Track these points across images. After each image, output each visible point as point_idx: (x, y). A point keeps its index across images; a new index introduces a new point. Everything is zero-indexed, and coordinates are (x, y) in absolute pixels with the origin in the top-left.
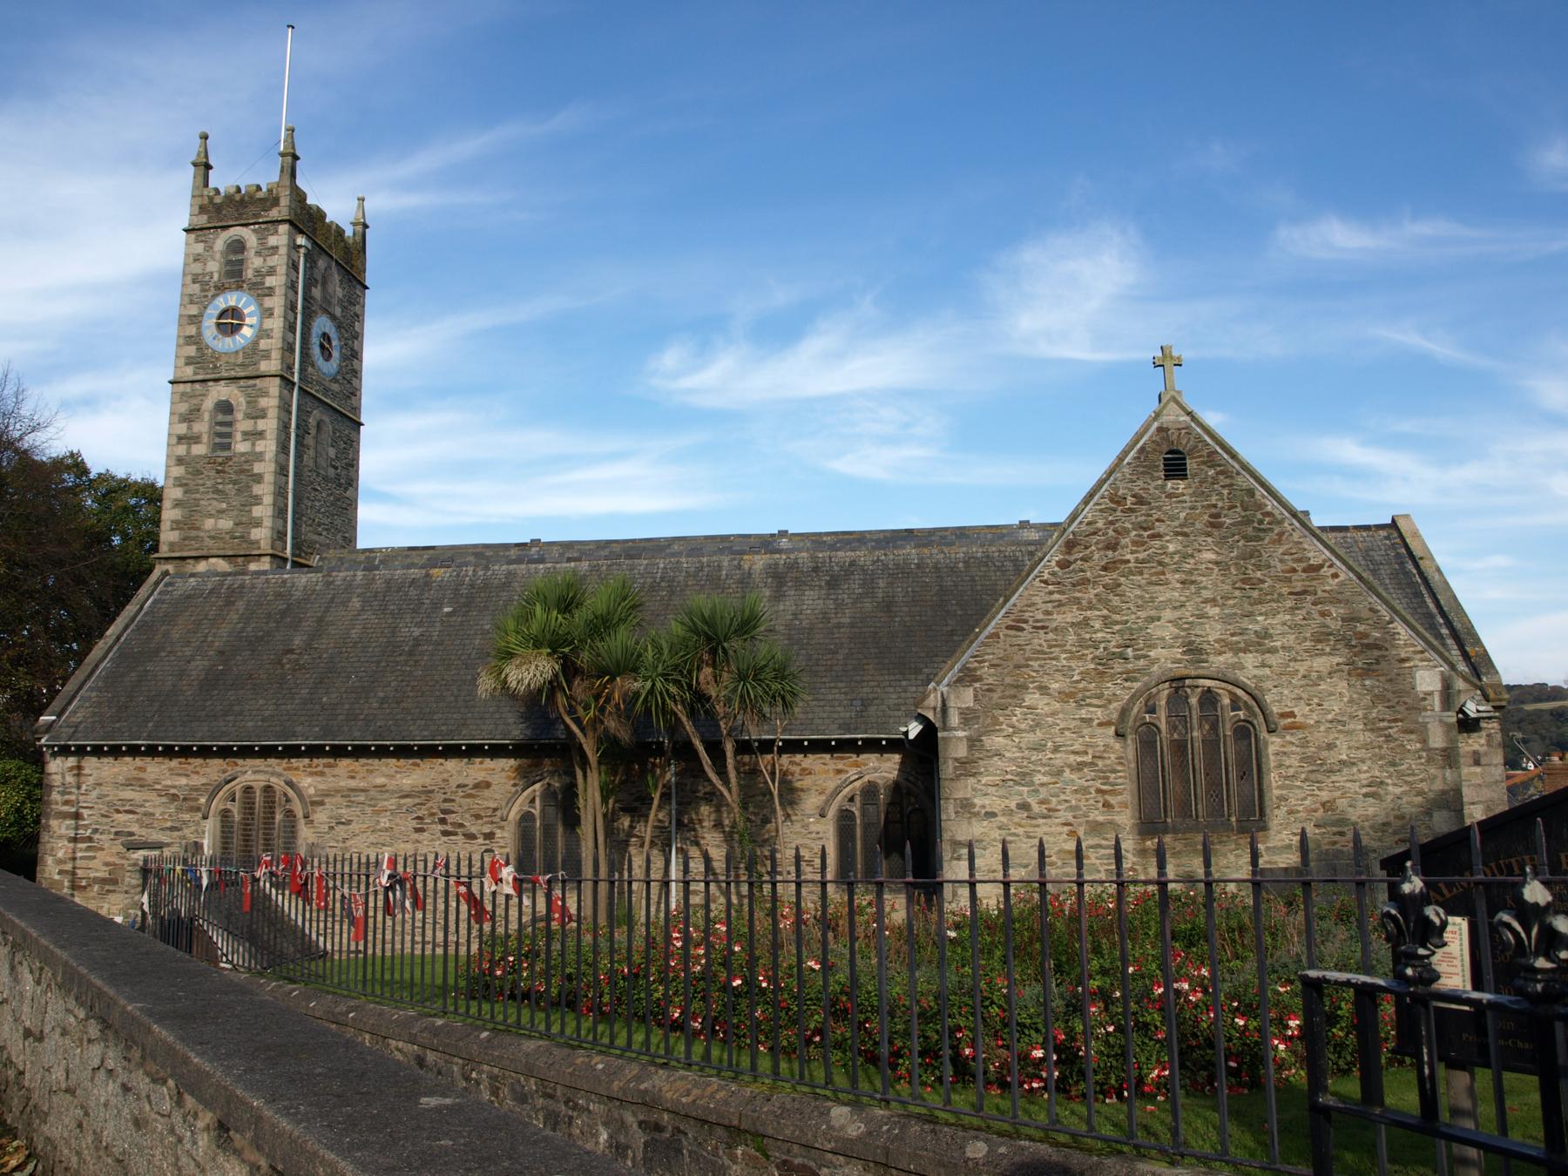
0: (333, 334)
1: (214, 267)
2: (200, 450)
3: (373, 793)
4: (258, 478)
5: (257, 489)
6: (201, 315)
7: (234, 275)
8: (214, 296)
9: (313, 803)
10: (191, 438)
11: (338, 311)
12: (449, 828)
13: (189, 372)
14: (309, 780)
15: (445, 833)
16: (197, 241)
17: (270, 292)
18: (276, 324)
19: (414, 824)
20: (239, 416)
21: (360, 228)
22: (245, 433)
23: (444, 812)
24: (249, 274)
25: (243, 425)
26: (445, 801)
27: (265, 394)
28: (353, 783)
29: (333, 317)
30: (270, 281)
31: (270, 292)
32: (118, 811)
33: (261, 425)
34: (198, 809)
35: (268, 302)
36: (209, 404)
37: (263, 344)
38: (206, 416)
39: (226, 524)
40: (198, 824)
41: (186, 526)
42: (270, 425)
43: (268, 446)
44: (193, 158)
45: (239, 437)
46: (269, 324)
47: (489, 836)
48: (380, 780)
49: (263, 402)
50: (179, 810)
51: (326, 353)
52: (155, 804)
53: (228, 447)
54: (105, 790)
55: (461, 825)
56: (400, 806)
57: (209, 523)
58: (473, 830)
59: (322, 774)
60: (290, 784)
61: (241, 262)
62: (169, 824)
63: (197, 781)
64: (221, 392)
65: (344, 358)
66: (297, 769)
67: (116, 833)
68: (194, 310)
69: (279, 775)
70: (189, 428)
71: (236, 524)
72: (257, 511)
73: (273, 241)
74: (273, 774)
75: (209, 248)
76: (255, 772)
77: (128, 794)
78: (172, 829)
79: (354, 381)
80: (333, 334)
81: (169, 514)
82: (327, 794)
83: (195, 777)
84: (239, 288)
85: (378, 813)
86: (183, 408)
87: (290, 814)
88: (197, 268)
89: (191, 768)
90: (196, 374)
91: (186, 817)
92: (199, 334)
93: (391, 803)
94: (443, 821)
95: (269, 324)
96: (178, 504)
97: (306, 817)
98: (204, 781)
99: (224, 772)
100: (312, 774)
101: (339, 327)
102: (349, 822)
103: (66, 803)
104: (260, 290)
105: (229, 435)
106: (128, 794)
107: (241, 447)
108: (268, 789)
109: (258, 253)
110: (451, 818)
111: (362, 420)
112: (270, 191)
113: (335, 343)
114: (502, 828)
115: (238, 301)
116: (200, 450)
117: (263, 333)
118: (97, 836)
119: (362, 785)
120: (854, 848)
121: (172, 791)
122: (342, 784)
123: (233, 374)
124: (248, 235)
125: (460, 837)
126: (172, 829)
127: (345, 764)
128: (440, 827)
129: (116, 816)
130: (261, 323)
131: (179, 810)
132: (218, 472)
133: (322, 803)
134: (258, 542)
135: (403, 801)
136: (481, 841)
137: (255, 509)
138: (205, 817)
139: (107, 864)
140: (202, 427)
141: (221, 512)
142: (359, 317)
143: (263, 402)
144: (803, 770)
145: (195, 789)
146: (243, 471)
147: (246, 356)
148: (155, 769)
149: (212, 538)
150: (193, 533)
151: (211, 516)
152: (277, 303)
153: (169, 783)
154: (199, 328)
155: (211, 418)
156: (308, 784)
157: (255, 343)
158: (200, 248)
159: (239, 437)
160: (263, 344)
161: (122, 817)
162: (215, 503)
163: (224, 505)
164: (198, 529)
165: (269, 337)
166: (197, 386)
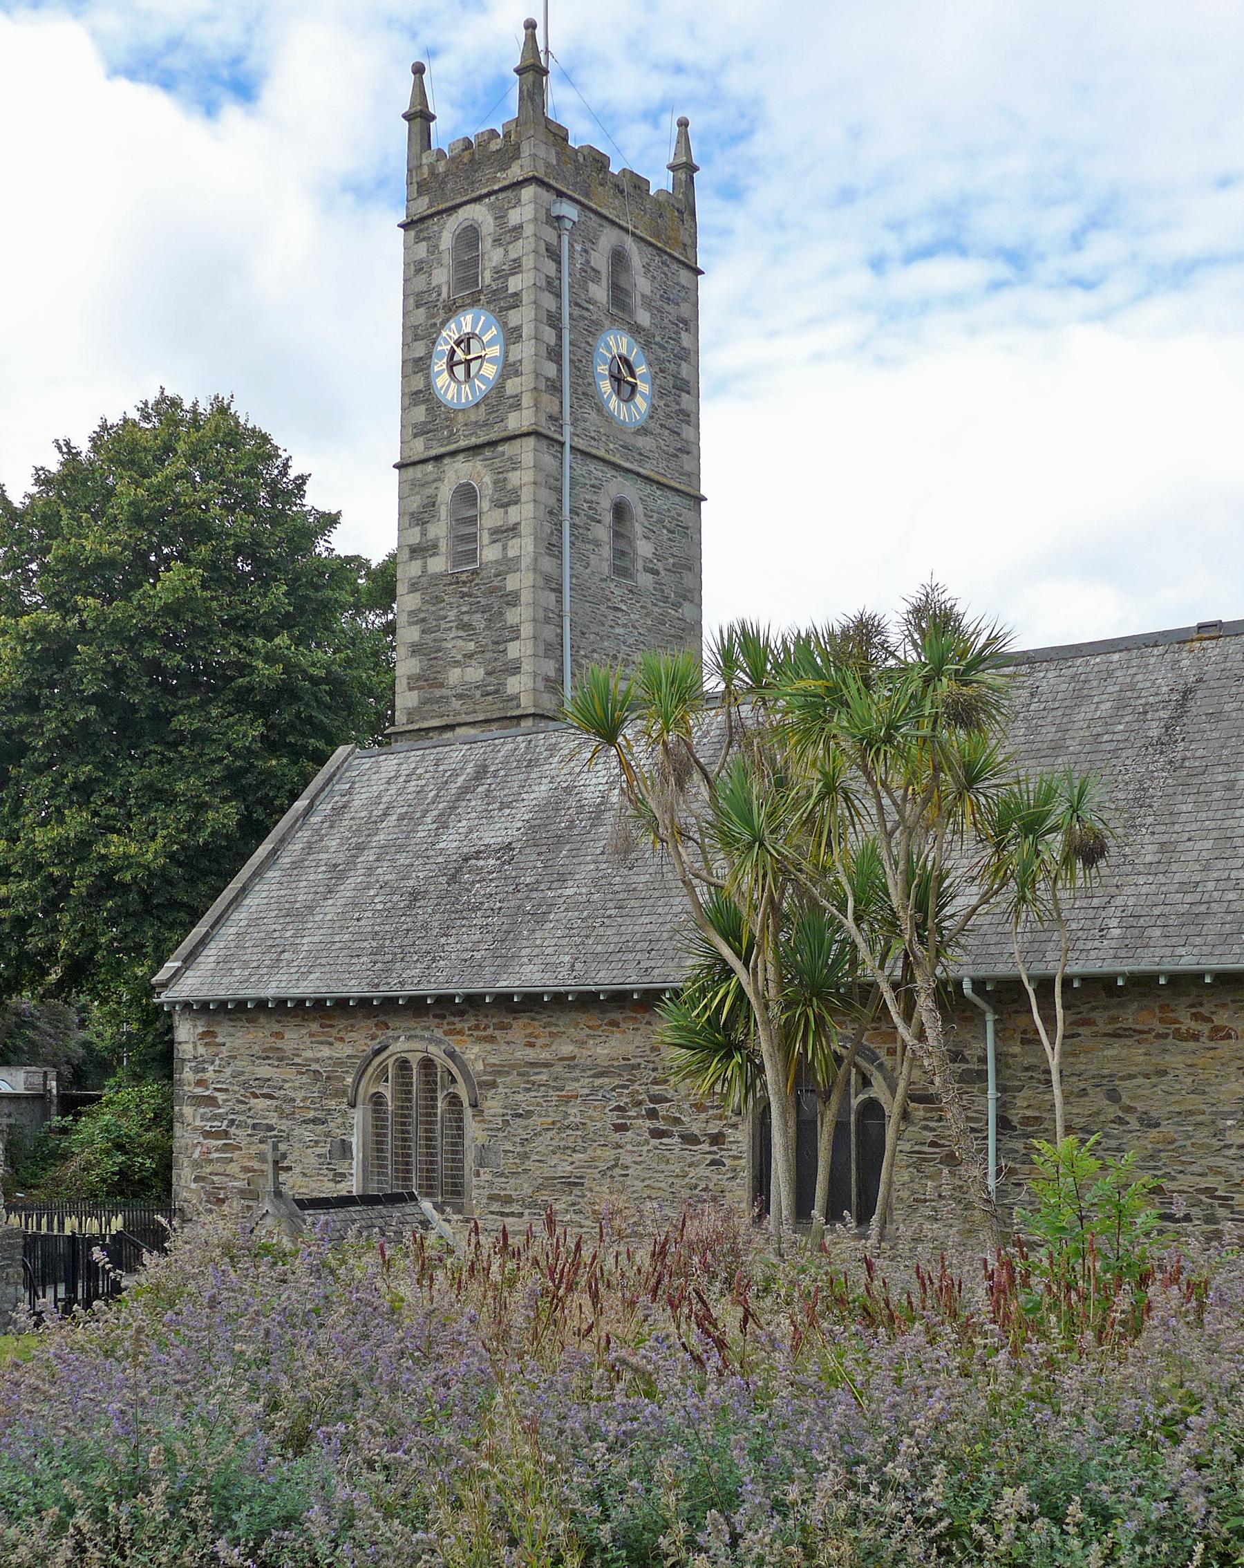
0: (634, 355)
1: (442, 276)
2: (438, 564)
3: (558, 1068)
4: (512, 600)
5: (512, 616)
6: (429, 356)
7: (470, 289)
8: (444, 323)
9: (482, 1085)
10: (425, 549)
11: (643, 318)
12: (661, 1125)
13: (419, 448)
14: (476, 1049)
15: (657, 1134)
16: (418, 240)
17: (515, 301)
18: (525, 351)
19: (613, 1118)
20: (485, 505)
21: (682, 175)
22: (495, 531)
23: (656, 1099)
24: (487, 278)
25: (491, 518)
26: (656, 1082)
27: (515, 465)
28: (531, 1054)
29: (635, 330)
30: (514, 284)
31: (515, 301)
32: (256, 1096)
33: (514, 515)
34: (344, 1093)
35: (514, 318)
36: (445, 492)
37: (512, 386)
38: (443, 512)
39: (475, 673)
40: (344, 1114)
41: (427, 681)
42: (523, 513)
43: (524, 547)
44: (406, 108)
45: (486, 537)
46: (516, 352)
47: (717, 1139)
48: (567, 1049)
49: (514, 478)
50: (324, 1095)
51: (623, 385)
52: (295, 1086)
53: (471, 556)
54: (239, 1064)
55: (677, 1121)
56: (594, 1090)
57: (454, 675)
58: (695, 1129)
59: (491, 1039)
60: (451, 1055)
61: (475, 260)
62: (311, 1115)
63: (343, 1050)
64: (459, 471)
65: (661, 392)
66: (460, 1033)
67: (254, 1126)
68: (419, 350)
69: (439, 1042)
70: (424, 534)
71: (488, 674)
72: (514, 650)
73: (514, 217)
74: (431, 1040)
75: (434, 249)
76: (408, 1038)
77: (265, 1071)
78: (314, 1121)
79: (687, 432)
80: (634, 355)
81: (405, 666)
82: (499, 1071)
83: (338, 1045)
84: (475, 302)
85: (567, 1100)
86: (415, 503)
87: (454, 1100)
88: (420, 283)
89: (334, 1032)
90: (427, 448)
91: (332, 1104)
92: (429, 385)
93: (581, 1086)
94: (652, 1114)
95: (516, 352)
96: (416, 649)
97: (474, 1105)
98: (349, 1051)
99: (373, 1038)
100: (481, 1040)
101: (646, 345)
102: (529, 1114)
103: (200, 1083)
104: (503, 302)
105: (473, 538)
106: (265, 1071)
107: (489, 553)
108: (428, 1064)
109: (497, 242)
110: (662, 1109)
111: (704, 491)
112: (507, 135)
113: (641, 369)
114: (734, 1126)
115: (475, 323)
116: (438, 564)
117: (509, 369)
118: (233, 1130)
119: (545, 1055)
120: (857, 1147)
121: (315, 1066)
122: (518, 1055)
123: (474, 441)
124: (479, 214)
125: (676, 1139)
126: (314, 1121)
127: (519, 1029)
128: (648, 1123)
129: (253, 1101)
130: (506, 354)
131: (324, 1095)
132: (463, 595)
133: (493, 1085)
134: (516, 697)
135: (598, 1082)
136: (705, 1147)
137: (510, 645)
138: (353, 1105)
139: (246, 1170)
140: (439, 530)
141: (470, 656)
142: (689, 323)
143: (514, 478)
144: (1216, 1029)
145: (338, 1063)
146: (493, 591)
147: (492, 409)
148: (294, 1037)
149: (459, 696)
150: (438, 693)
151: (457, 663)
152: (523, 317)
153: (309, 1054)
154: (427, 377)
155: (452, 513)
156: (474, 1054)
157: (499, 387)
158: (422, 250)
159: (486, 537)
160: (512, 386)
161: (260, 1104)
162: (460, 643)
163: (472, 646)
164: (441, 685)
165: (518, 373)
166: (430, 467)
